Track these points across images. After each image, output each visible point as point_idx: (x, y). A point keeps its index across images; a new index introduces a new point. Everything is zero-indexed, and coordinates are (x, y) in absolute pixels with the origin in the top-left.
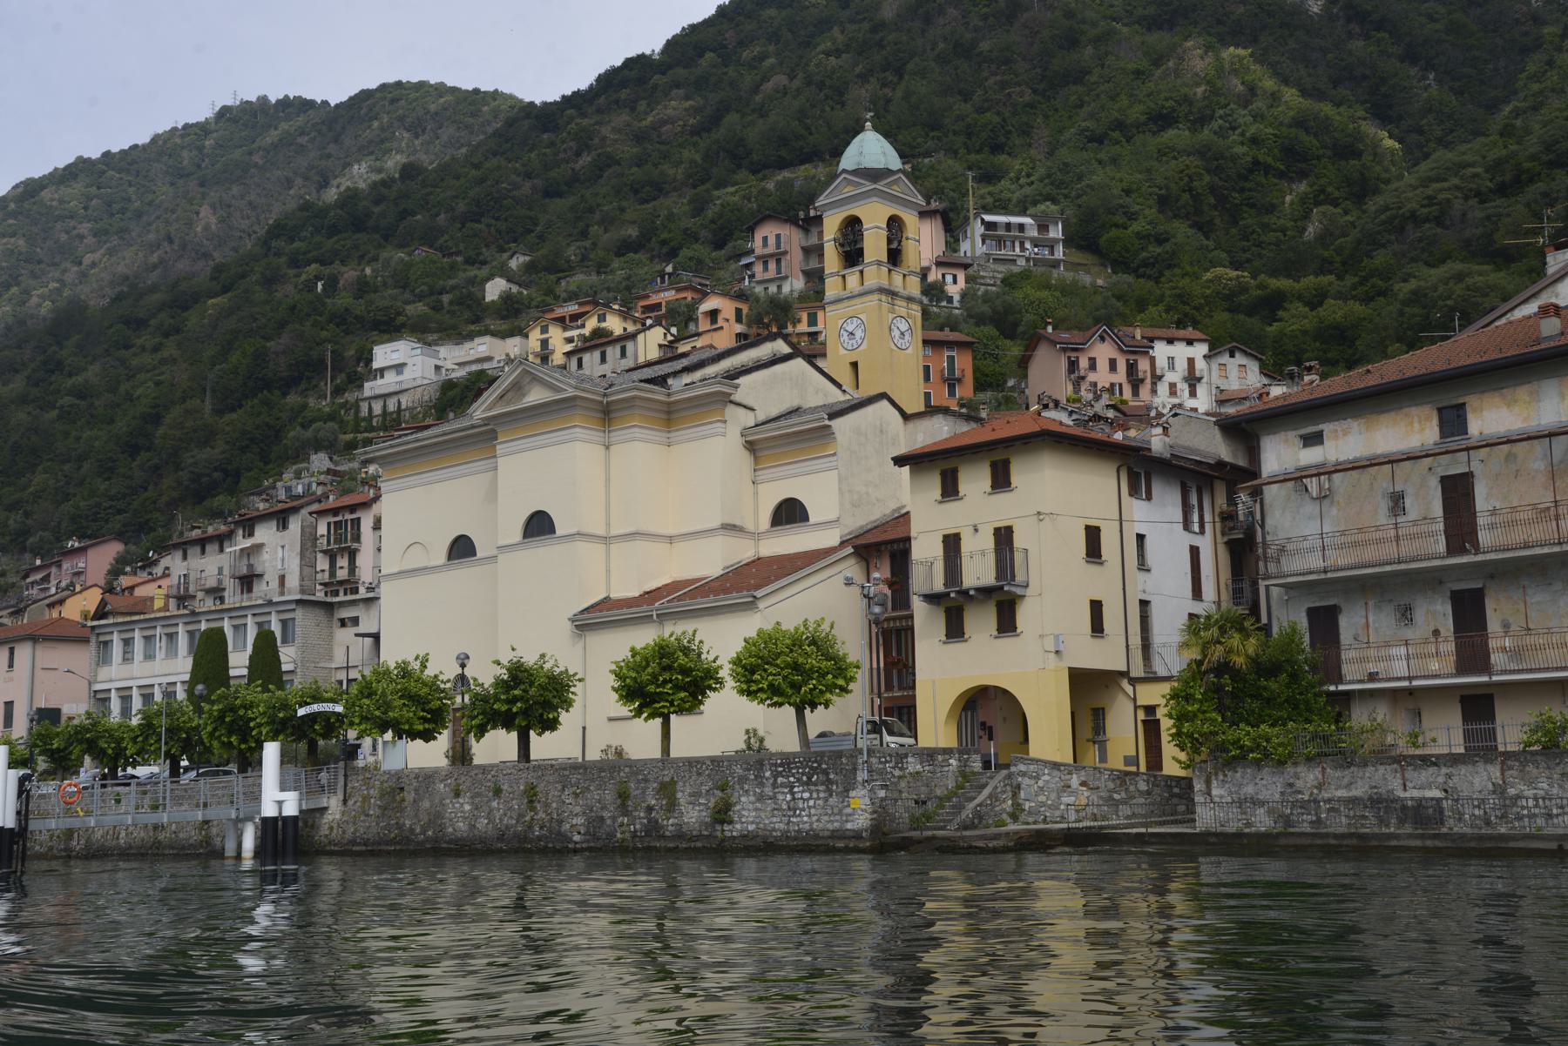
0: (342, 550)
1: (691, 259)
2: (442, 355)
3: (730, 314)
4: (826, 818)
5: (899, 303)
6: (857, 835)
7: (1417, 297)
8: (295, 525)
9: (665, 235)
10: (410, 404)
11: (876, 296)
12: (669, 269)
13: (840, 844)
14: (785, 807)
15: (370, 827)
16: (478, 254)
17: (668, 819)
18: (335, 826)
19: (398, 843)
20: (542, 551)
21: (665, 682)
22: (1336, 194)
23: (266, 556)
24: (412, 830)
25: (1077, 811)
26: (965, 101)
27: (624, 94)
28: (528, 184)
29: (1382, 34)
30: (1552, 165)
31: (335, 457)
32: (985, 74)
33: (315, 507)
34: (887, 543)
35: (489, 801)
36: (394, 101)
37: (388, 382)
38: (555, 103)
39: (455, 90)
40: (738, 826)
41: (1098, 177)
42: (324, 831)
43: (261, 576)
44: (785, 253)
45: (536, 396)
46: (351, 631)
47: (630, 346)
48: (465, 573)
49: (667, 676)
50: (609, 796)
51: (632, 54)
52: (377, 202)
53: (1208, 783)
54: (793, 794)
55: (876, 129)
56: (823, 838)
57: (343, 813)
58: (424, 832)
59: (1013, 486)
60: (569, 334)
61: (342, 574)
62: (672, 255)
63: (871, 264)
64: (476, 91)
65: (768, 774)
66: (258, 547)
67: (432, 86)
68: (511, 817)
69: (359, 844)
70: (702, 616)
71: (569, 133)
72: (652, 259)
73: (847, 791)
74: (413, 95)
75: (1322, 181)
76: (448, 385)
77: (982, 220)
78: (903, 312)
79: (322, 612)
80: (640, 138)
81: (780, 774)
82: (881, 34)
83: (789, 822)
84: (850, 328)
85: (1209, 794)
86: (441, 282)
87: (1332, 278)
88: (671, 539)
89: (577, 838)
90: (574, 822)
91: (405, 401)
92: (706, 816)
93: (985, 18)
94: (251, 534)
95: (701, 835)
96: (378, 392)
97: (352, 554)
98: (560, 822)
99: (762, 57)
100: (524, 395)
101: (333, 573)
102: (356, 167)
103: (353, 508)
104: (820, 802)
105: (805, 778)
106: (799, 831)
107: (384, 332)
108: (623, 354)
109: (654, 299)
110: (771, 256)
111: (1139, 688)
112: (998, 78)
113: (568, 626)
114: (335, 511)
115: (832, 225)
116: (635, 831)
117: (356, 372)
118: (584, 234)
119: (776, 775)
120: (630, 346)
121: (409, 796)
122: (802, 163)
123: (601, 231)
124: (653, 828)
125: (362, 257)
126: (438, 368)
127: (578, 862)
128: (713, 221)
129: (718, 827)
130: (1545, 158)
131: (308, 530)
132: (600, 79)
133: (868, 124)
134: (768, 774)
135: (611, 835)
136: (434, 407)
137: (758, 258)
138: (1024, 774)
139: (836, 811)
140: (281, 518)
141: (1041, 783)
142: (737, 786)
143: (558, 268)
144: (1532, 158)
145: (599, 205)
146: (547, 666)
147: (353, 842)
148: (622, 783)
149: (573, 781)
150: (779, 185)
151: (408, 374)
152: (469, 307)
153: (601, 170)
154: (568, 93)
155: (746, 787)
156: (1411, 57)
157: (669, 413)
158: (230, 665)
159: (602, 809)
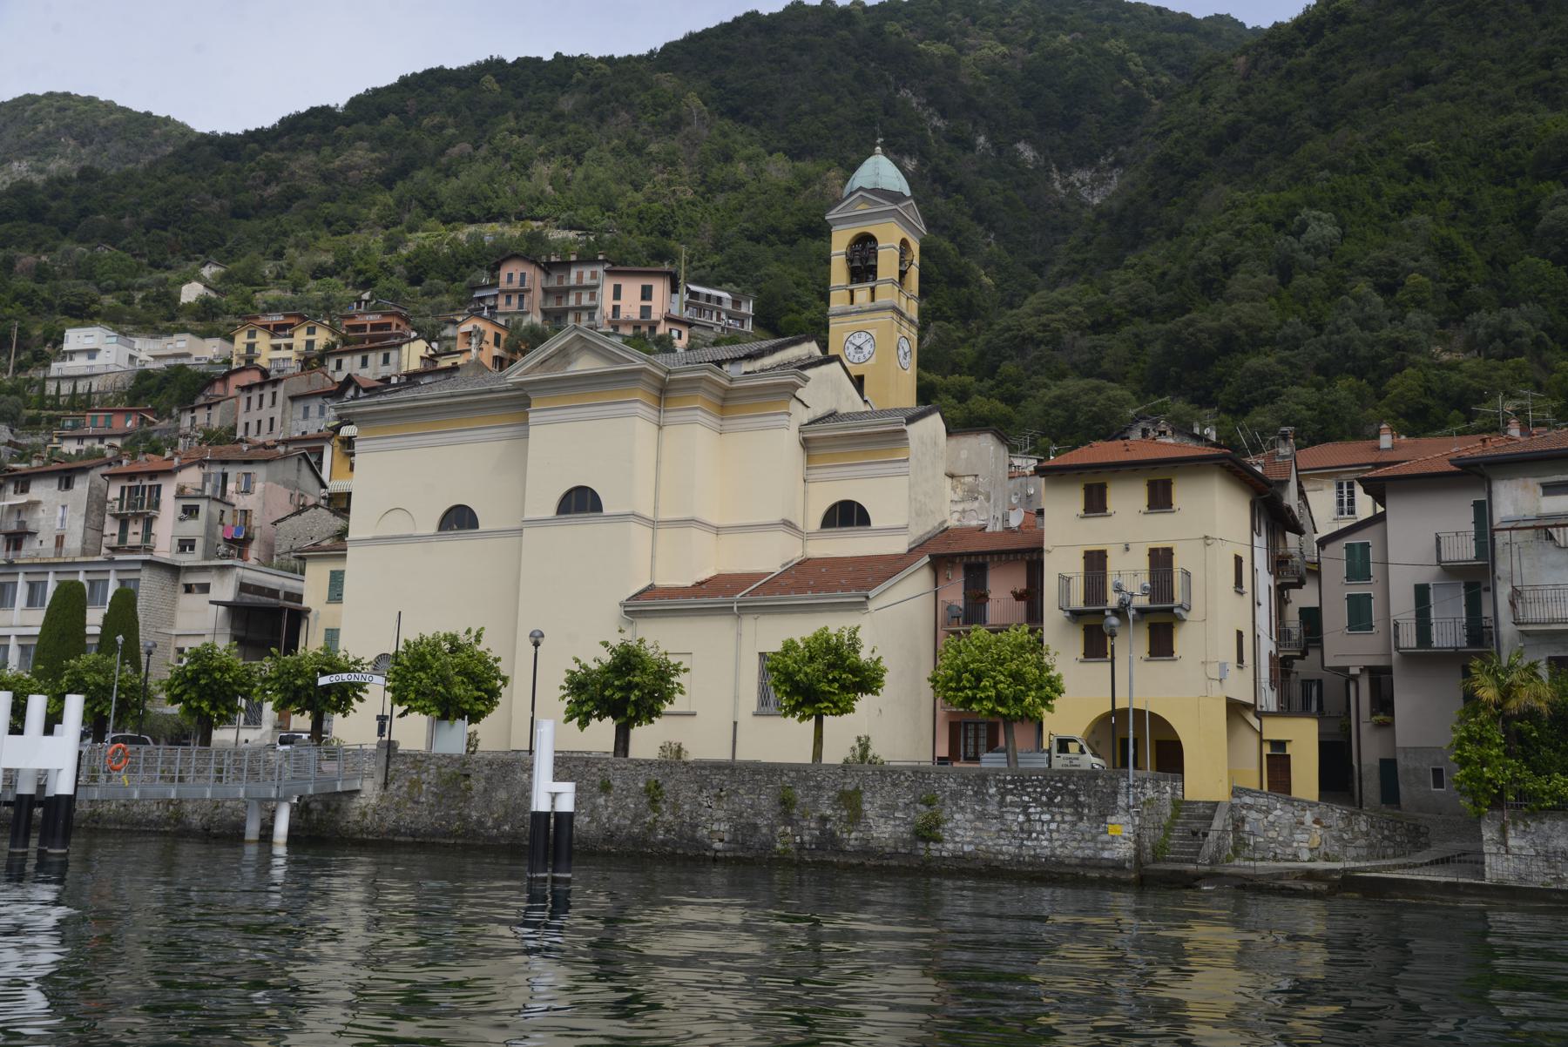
0: (137, 516)
1: (389, 290)
2: (137, 346)
3: (489, 337)
4: (1074, 844)
5: (904, 323)
6: (1118, 865)
7: (1060, 401)
8: (81, 486)
9: (361, 266)
10: (101, 389)
11: (889, 314)
12: (366, 296)
13: (1095, 874)
14: (1016, 828)
15: (420, 815)
16: (164, 259)
17: (850, 832)
18: (370, 812)
19: (460, 836)
20: (581, 529)
21: (835, 680)
22: (949, 313)
23: (40, 514)
24: (480, 823)
25: (1311, 850)
26: (636, 190)
27: (308, 138)
28: (216, 203)
29: (959, 197)
30: (1135, 313)
31: (16, 430)
32: (653, 171)
33: (105, 470)
34: (961, 555)
35: (594, 796)
36: (61, 109)
37: (79, 365)
38: (237, 136)
39: (125, 110)
40: (950, 846)
41: (774, 268)
42: (355, 816)
43: (33, 534)
44: (528, 291)
45: (585, 364)
46: (198, 600)
47: (393, 354)
48: (460, 545)
49: (836, 674)
50: (766, 801)
51: (318, 103)
52: (55, 197)
53: (1503, 832)
54: (1027, 815)
55: (886, 154)
56: (1069, 865)
57: (382, 798)
58: (498, 825)
59: (1175, 507)
60: (276, 341)
61: (134, 539)
62: (367, 285)
63: (884, 282)
64: (148, 114)
65: (992, 791)
66: (34, 505)
67: (101, 102)
68: (625, 818)
69: (405, 834)
70: (851, 610)
71: (258, 163)
72: (347, 285)
73: (1105, 816)
74: (82, 107)
75: (940, 301)
76: (144, 375)
77: (688, 289)
78: (906, 333)
79: (168, 575)
80: (326, 178)
81: (1011, 792)
82: (562, 123)
83: (1021, 845)
84: (858, 342)
85: (1505, 844)
86: (129, 280)
87: (972, 379)
88: (718, 530)
89: (718, 845)
90: (715, 827)
91: (96, 385)
92: (904, 832)
93: (653, 125)
94: (25, 490)
95: (897, 853)
96: (66, 373)
97: (149, 522)
98: (694, 827)
99: (442, 127)
100: (569, 363)
101: (123, 538)
102: (16, 164)
103: (153, 475)
104: (1066, 826)
105: (1044, 798)
106: (1036, 856)
107: (76, 317)
108: (386, 361)
109: (359, 321)
110: (515, 291)
111: (1266, 722)
112: (665, 176)
113: (620, 610)
114: (131, 476)
115: (840, 241)
116: (802, 842)
117: (43, 352)
118: (279, 255)
119: (1003, 793)
120: (393, 354)
121: (478, 785)
122: (489, 221)
123: (297, 254)
124: (828, 840)
125: (38, 246)
126: (132, 358)
127: (718, 877)
128: (408, 260)
129: (921, 845)
130: (1130, 307)
131: (95, 492)
132: (283, 121)
133: (878, 148)
134: (992, 791)
135: (768, 845)
136: (127, 393)
137: (502, 292)
138: (1250, 807)
139: (1087, 837)
140: (66, 478)
141: (1271, 818)
142: (948, 802)
143: (253, 281)
144: (1120, 305)
145: (293, 231)
146: (480, 648)
147: (396, 831)
148: (784, 788)
149: (715, 782)
150: (470, 236)
151: (100, 360)
152: (165, 304)
153: (289, 200)
154: (252, 128)
155: (962, 803)
156: (978, 218)
157: (724, 399)
158: (88, 622)
159: (755, 815)
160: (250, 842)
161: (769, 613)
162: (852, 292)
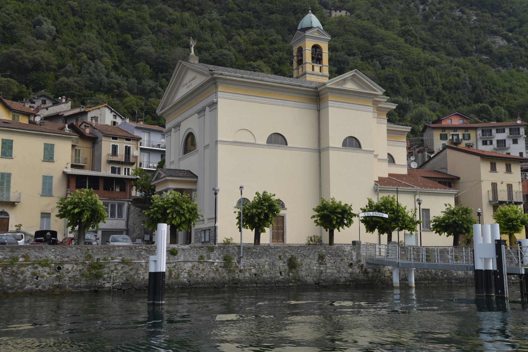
48: (277, 152)
59: (512, 172)
160: (397, 288)
161: (424, 195)
162: (313, 66)
